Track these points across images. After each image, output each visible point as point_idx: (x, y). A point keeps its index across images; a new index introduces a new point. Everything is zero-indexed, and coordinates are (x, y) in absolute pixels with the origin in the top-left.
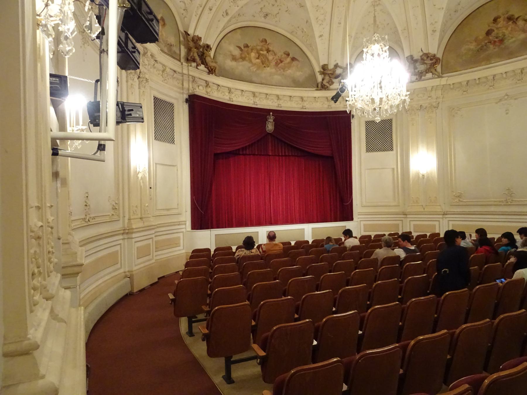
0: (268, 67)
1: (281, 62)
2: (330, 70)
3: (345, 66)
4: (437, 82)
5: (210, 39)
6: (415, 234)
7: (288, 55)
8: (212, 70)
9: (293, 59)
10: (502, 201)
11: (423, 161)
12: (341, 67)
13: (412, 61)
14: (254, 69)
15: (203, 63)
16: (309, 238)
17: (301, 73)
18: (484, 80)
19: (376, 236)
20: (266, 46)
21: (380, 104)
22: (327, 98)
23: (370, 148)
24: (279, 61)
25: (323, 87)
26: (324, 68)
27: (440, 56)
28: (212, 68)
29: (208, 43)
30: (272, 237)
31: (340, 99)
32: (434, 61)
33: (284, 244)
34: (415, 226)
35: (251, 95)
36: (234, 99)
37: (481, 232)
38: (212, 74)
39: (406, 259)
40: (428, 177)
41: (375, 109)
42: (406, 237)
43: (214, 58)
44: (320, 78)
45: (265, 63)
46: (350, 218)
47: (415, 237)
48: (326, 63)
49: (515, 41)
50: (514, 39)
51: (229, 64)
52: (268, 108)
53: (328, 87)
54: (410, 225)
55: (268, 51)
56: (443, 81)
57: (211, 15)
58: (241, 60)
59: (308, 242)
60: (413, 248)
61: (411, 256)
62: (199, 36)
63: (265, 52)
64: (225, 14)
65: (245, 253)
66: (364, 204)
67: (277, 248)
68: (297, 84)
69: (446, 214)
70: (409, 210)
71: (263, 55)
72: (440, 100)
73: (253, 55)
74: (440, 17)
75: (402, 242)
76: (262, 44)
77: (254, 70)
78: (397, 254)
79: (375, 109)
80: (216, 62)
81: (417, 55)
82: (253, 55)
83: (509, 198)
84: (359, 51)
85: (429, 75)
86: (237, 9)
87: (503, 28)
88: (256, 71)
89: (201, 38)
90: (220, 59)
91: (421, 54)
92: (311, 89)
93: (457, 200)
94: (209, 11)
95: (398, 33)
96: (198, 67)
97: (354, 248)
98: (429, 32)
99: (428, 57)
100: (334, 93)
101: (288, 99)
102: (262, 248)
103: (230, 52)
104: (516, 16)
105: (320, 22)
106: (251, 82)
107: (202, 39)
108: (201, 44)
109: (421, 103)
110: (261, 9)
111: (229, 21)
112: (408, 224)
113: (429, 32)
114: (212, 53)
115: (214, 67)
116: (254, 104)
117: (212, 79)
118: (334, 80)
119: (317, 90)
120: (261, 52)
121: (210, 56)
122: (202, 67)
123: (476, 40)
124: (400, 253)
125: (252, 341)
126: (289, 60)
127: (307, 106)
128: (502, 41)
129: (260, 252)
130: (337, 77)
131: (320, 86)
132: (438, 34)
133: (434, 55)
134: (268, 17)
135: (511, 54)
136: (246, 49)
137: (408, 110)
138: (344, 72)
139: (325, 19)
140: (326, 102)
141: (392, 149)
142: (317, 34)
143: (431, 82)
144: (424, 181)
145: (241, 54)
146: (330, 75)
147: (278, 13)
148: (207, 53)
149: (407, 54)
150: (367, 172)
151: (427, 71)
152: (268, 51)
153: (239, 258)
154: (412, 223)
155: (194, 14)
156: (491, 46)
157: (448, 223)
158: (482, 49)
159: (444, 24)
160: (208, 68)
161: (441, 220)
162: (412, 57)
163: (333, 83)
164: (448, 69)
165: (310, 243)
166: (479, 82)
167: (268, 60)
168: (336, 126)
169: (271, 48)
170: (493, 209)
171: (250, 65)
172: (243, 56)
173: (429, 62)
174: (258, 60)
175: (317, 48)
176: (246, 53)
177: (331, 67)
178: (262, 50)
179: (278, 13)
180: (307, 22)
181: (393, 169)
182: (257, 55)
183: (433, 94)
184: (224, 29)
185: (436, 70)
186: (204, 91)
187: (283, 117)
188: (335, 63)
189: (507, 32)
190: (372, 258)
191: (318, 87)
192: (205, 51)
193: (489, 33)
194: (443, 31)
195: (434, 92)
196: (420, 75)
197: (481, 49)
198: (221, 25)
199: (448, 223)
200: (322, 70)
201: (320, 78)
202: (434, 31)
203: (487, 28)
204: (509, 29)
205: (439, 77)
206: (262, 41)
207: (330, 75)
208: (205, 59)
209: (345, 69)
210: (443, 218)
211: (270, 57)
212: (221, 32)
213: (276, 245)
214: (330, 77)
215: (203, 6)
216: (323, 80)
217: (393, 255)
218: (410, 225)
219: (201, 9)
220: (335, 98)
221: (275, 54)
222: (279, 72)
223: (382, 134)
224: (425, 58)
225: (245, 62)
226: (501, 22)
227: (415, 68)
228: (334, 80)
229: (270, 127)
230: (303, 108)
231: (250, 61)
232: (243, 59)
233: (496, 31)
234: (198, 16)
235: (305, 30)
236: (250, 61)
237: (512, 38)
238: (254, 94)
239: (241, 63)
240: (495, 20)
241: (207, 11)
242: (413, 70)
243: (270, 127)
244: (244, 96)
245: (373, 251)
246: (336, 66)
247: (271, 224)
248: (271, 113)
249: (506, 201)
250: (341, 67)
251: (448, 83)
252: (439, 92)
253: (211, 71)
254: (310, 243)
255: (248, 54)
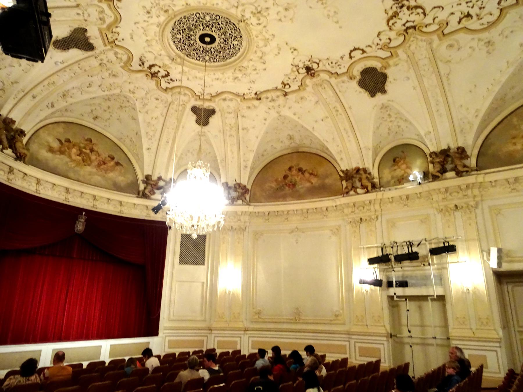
0: (89, 165)
1: (104, 163)
2: (154, 181)
3: (168, 180)
4: (245, 208)
5: (28, 128)
6: (218, 351)
7: (113, 159)
8: (21, 156)
9: (117, 164)
10: (292, 319)
11: (229, 276)
12: (164, 180)
13: (226, 185)
14: (73, 165)
15: (10, 147)
16: (106, 357)
17: (123, 178)
18: (282, 213)
19: (181, 354)
20: (90, 146)
21: (198, 221)
22: (147, 206)
23: (184, 260)
24: (102, 163)
25: (144, 196)
26: (148, 178)
27: (249, 187)
28: (22, 154)
29: (23, 128)
30: (59, 357)
31: (160, 211)
32: (244, 191)
33: (72, 366)
34: (219, 342)
35: (63, 190)
36: (42, 192)
37: (276, 350)
38: (20, 161)
39: (211, 381)
40: (233, 294)
41: (193, 226)
42: (210, 354)
43: (26, 144)
44: (142, 186)
45: (86, 161)
46: (154, 332)
47: (218, 354)
48: (150, 173)
49: (302, 188)
50: (302, 186)
51: (44, 154)
52: (81, 207)
53: (149, 196)
54: (214, 341)
55: (92, 150)
56: (251, 209)
57: (32, 103)
58: (58, 153)
59: (104, 362)
60: (217, 368)
61: (215, 377)
62: (14, 119)
63: (88, 151)
64: (50, 106)
65: (20, 381)
66: (172, 317)
67: (65, 373)
68: (117, 188)
69: (247, 330)
70: (214, 325)
71: (85, 153)
72: (248, 224)
73: (74, 151)
74: (251, 157)
75: (207, 362)
76: (86, 142)
77: (73, 166)
78: (201, 376)
79: (193, 226)
80: (28, 150)
81: (231, 183)
82: (74, 151)
83: (297, 316)
84: (182, 169)
85: (240, 202)
86: (65, 104)
87: (296, 177)
88: (74, 167)
89: (15, 121)
90: (34, 147)
91: (235, 183)
92: (131, 195)
93: (257, 317)
94: (32, 99)
95: (217, 162)
96: (4, 151)
97: (156, 370)
98: (242, 167)
99: (240, 186)
100: (155, 204)
101: (106, 201)
102: (44, 375)
103: (48, 142)
104: (304, 169)
105: (150, 137)
106: (67, 177)
107: (17, 123)
108: (14, 127)
109: (232, 224)
110: (92, 111)
111: (53, 113)
112: (213, 339)
113: (242, 167)
114: (25, 140)
115: (24, 154)
116: (66, 200)
117: (19, 166)
118: (156, 191)
119: (137, 197)
120: (84, 150)
121: (22, 142)
122: (9, 151)
123: (276, 181)
124: (204, 374)
125: (344, 369)
126: (112, 163)
127: (125, 211)
128: (294, 185)
129: (41, 380)
130: (159, 188)
131: (141, 193)
132: (248, 170)
133: (245, 186)
134: (97, 120)
135: (300, 197)
136: (67, 144)
137: (220, 230)
138: (166, 185)
139: (154, 135)
140: (145, 211)
141: (203, 264)
142: (145, 146)
143: (241, 208)
144: (231, 299)
145: (60, 148)
146: (153, 186)
147: (109, 119)
148: (19, 138)
149: (223, 180)
150: (179, 286)
151: (239, 198)
152: (92, 150)
153: (8, 389)
154: (217, 339)
155: (13, 96)
156: (287, 188)
157: (249, 339)
158: (280, 189)
159: (254, 163)
160: (16, 154)
161: (242, 336)
162: (227, 184)
163: (154, 193)
164: (254, 200)
165: (107, 364)
166: (277, 214)
167: (90, 159)
168: (151, 236)
169: (95, 148)
170: (285, 326)
171: (68, 160)
172: (63, 149)
173: (240, 191)
174: (79, 158)
175: (143, 158)
176: (66, 148)
177: (155, 178)
178: (85, 148)
179: (109, 119)
180: (136, 134)
181: (203, 283)
182: (79, 152)
183: (242, 218)
184: (45, 119)
185: (245, 198)
186: (5, 178)
187: (94, 217)
188: (158, 176)
189: (298, 179)
190: (175, 382)
191: (139, 194)
192: (17, 136)
193: (285, 177)
194: (253, 169)
195: (242, 217)
196: (233, 200)
197: (280, 188)
198: (43, 115)
199: (249, 339)
200: (145, 180)
201: (142, 186)
202: (246, 167)
203: (284, 173)
204: (299, 177)
205: (247, 205)
206: (87, 140)
207: (153, 186)
208: (15, 144)
209: (168, 183)
210: (244, 334)
211: (93, 157)
212: (41, 121)
213: (64, 368)
214: (151, 186)
215: (26, 92)
216: (145, 188)
217: (197, 377)
218: (214, 341)
219: (23, 94)
220: (156, 210)
221: (99, 155)
222: (100, 173)
223: (195, 249)
224: (238, 187)
225: (62, 156)
226: (294, 172)
227: (229, 194)
228: (156, 191)
229: (80, 227)
230: (120, 212)
231: (70, 156)
232: (62, 152)
233: (290, 177)
234: (17, 100)
235: (134, 140)
236: (70, 156)
237: (301, 184)
238: (67, 190)
239: (58, 156)
240: (290, 169)
241: (29, 96)
242: (227, 195)
243: (80, 227)
244: (54, 190)
245: (178, 373)
246: (160, 178)
247: (60, 339)
248: (84, 213)
249: (295, 319)
250: (164, 180)
251: (255, 211)
252: (247, 218)
253: (19, 157)
254: (107, 364)
255: (69, 148)
